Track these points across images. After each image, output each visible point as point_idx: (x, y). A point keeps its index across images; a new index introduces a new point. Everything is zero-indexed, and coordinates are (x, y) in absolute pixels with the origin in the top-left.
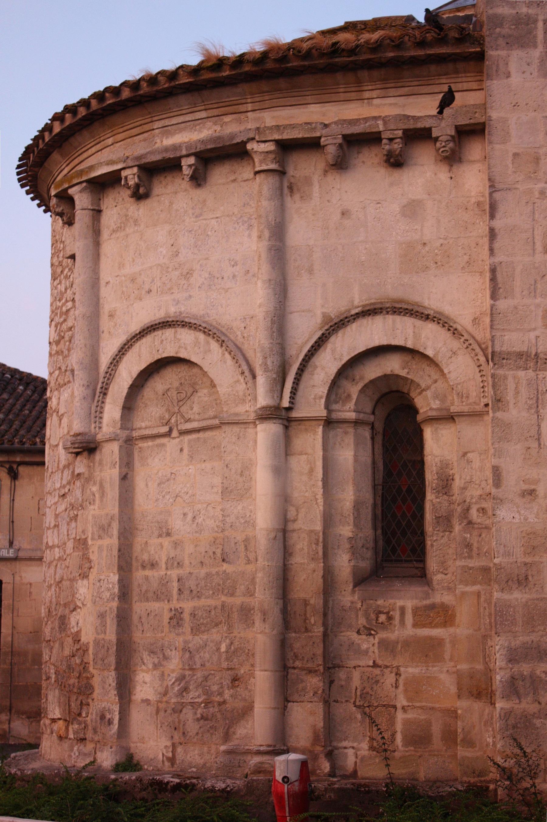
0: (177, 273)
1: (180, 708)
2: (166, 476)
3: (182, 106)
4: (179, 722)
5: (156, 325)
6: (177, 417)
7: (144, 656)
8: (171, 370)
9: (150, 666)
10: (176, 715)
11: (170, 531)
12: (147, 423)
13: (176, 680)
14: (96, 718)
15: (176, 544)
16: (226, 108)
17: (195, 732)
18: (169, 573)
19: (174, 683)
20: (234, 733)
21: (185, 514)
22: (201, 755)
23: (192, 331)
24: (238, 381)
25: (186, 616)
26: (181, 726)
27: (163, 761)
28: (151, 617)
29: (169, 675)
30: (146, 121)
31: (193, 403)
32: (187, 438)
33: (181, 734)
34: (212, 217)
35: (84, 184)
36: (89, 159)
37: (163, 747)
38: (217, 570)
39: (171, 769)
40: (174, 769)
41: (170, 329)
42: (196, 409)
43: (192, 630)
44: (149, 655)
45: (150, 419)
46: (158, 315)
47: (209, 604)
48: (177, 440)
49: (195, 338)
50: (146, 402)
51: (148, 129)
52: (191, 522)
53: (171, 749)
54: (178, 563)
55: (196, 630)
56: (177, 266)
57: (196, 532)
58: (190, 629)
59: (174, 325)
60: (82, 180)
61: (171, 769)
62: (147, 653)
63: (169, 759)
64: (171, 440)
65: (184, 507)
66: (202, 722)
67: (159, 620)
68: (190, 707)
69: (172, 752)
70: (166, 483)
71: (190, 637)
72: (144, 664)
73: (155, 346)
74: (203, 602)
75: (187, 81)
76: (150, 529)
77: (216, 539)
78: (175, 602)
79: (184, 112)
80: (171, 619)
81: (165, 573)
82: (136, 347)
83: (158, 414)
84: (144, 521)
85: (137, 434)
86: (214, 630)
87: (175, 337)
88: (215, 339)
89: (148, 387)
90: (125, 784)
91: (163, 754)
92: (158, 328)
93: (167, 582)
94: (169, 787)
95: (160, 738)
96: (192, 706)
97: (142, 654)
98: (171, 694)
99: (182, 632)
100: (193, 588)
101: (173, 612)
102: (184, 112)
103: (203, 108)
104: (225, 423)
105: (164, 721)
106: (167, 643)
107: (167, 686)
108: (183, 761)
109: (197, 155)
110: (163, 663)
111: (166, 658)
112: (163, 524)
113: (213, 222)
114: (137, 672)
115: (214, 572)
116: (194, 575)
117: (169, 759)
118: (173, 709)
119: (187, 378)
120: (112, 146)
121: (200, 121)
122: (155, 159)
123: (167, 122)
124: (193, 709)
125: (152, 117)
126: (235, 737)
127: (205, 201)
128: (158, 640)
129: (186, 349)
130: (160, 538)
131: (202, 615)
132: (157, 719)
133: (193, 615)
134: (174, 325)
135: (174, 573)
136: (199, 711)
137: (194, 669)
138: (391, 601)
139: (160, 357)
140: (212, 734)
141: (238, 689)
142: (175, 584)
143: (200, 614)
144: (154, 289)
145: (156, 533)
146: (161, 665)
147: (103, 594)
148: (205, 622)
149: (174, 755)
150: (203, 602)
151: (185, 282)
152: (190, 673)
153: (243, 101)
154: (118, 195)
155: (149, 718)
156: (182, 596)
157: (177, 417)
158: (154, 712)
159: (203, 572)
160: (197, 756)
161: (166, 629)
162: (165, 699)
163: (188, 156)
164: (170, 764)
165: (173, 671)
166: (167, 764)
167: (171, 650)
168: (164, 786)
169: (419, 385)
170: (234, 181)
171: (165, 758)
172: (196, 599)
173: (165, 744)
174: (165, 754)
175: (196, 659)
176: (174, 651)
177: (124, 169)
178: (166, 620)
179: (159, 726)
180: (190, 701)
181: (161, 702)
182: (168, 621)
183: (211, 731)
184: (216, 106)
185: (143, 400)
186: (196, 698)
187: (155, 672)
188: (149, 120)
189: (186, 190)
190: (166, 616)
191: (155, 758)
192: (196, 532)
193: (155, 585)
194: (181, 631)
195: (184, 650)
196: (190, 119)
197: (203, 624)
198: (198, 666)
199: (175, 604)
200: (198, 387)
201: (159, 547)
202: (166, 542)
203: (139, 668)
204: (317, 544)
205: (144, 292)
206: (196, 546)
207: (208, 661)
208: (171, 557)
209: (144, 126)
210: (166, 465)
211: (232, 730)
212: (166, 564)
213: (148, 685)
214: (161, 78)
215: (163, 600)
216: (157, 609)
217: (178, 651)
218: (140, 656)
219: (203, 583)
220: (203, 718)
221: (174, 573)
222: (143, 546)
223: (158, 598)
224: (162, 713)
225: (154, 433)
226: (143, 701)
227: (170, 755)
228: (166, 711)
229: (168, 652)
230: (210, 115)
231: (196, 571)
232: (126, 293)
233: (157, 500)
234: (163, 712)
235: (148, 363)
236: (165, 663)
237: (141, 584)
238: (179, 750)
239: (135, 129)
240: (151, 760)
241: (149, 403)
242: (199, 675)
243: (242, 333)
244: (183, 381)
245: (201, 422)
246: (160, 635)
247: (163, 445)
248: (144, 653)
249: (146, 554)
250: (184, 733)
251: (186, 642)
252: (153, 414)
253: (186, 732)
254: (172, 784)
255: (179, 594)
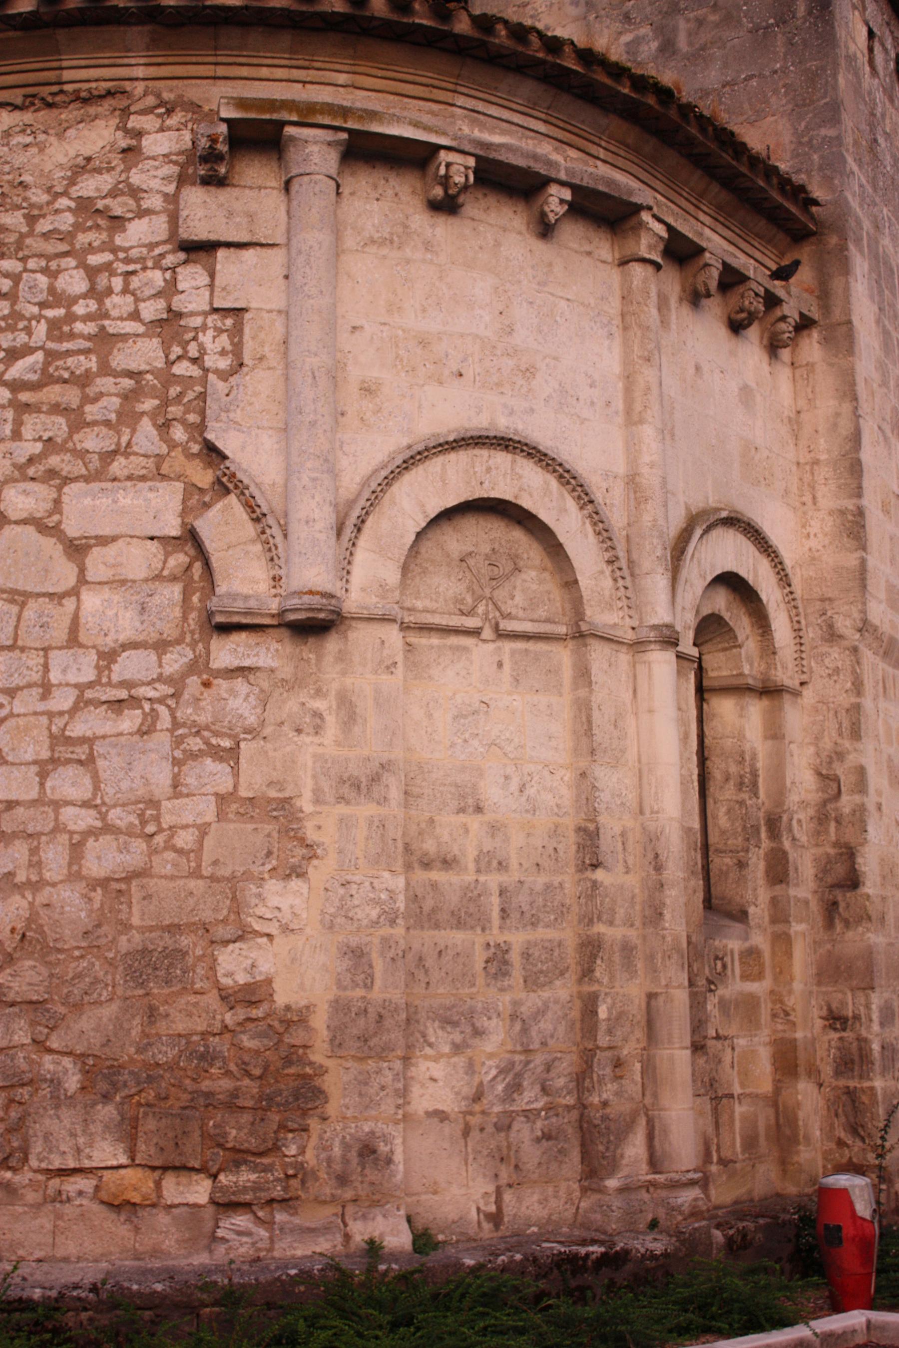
0: (511, 363)
1: (507, 1122)
2: (470, 705)
3: (515, 95)
4: (509, 1147)
5: (487, 437)
6: (487, 605)
7: (430, 1031)
8: (474, 522)
9: (446, 1049)
10: (503, 1134)
11: (481, 805)
12: (428, 604)
13: (500, 1072)
14: (344, 1157)
15: (494, 829)
16: (573, 137)
17: (536, 1161)
18: (482, 879)
19: (495, 1078)
20: (622, 1156)
21: (507, 778)
22: (543, 1202)
23: (539, 470)
24: (602, 572)
25: (515, 957)
26: (512, 1153)
27: (479, 1222)
28: (447, 958)
29: (484, 1063)
30: (444, 85)
31: (515, 588)
32: (508, 646)
33: (512, 1168)
34: (561, 294)
35: (345, 136)
36: (257, 83)
37: (479, 1196)
38: (559, 879)
39: (495, 1234)
40: (500, 1234)
41: (504, 454)
42: (519, 599)
43: (525, 981)
44: (443, 1028)
45: (434, 597)
46: (504, 424)
47: (549, 937)
48: (491, 646)
49: (545, 482)
50: (424, 565)
51: (441, 99)
52: (517, 793)
53: (493, 1199)
54: (500, 863)
55: (532, 982)
56: (510, 351)
57: (527, 811)
58: (521, 981)
59: (515, 448)
60: (345, 125)
61: (495, 1234)
62: (437, 1024)
63: (490, 1217)
64: (480, 643)
65: (505, 765)
66: (545, 1143)
67: (464, 964)
68: (523, 1119)
69: (496, 1203)
70: (470, 718)
71: (523, 995)
72: (430, 1045)
73: (475, 473)
74: (542, 933)
75: (574, 67)
76: (438, 795)
77: (557, 826)
78: (495, 931)
79: (514, 106)
80: (487, 962)
81: (475, 878)
82: (436, 464)
83: (451, 591)
84: (424, 780)
85: (412, 618)
86: (558, 983)
87: (512, 470)
88: (576, 494)
89: (429, 539)
90: (502, 1271)
91: (478, 1209)
92: (484, 444)
93: (479, 895)
94: (590, 1263)
95: (474, 1180)
96: (526, 1117)
97: (426, 1027)
98: (491, 1098)
99: (509, 986)
100: (525, 908)
101: (493, 950)
102: (514, 106)
103: (543, 116)
104: (596, 636)
105: (479, 1149)
106: (480, 1005)
107: (481, 1084)
108: (515, 1215)
109: (575, 188)
110: (470, 1042)
111: (478, 1033)
112: (467, 790)
113: (563, 304)
114: (413, 1061)
115: (556, 884)
116: (526, 886)
117: (490, 1217)
118: (495, 1124)
119: (503, 543)
120: (341, 89)
121: (532, 134)
122: (515, 162)
123: (480, 106)
124: (528, 1122)
125: (456, 84)
126: (624, 1162)
127: (550, 264)
128: (461, 999)
129: (531, 495)
130: (461, 815)
131: (540, 956)
132: (466, 1146)
133: (526, 955)
134: (515, 448)
135: (493, 880)
136: (539, 1124)
137: (530, 1051)
138: (724, 941)
139: (486, 496)
140: (561, 1162)
141: (623, 1082)
142: (495, 900)
143: (537, 954)
144: (469, 374)
145: (454, 804)
146: (468, 1046)
147: (357, 910)
148: (544, 968)
149: (499, 1208)
150: (542, 933)
151: (523, 382)
152: (523, 1058)
153: (596, 140)
154: (383, 182)
155: (446, 1145)
156: (508, 921)
157: (487, 605)
158: (459, 1133)
159: (540, 881)
160: (536, 1205)
161: (480, 980)
162: (477, 1108)
163: (563, 184)
164: (491, 1225)
165: (491, 1056)
166: (487, 1226)
167: (490, 1018)
168: (581, 1262)
169: (736, 637)
170: (589, 254)
171: (482, 1216)
172: (529, 928)
173: (484, 1190)
174: (483, 1208)
175: (534, 1034)
176: (495, 1021)
177: (449, 149)
178: (479, 965)
179: (471, 1157)
180: (524, 1107)
181: (471, 1113)
182: (483, 965)
183: (560, 1159)
184: (561, 124)
185: (418, 561)
186: (533, 1102)
187: (455, 1059)
188: (451, 86)
189: (520, 233)
190: (479, 957)
191: (461, 1218)
192: (527, 811)
193: (453, 899)
194: (506, 983)
195: (514, 1017)
196: (521, 123)
197: (541, 972)
198: (535, 1045)
199: (496, 936)
200: (521, 564)
201: (461, 831)
202: (475, 823)
203: (418, 1054)
204: (695, 850)
205: (446, 372)
206: (528, 835)
207: (552, 1036)
208: (485, 851)
209: (435, 91)
210: (471, 684)
211: (619, 1151)
212: (477, 861)
213: (441, 1083)
214: (534, 38)
215: (472, 928)
216: (459, 943)
217: (503, 1020)
218: (419, 1031)
219: (540, 901)
220: (547, 1136)
221: (493, 880)
222: (423, 825)
223: (460, 924)
224: (475, 1134)
225: (451, 624)
226: (430, 1114)
227: (493, 1208)
228: (482, 1130)
229: (482, 1022)
230: (551, 134)
231: (531, 879)
232: (405, 361)
233: (453, 745)
234: (478, 1132)
235: (462, 499)
236: (476, 1042)
237: (420, 896)
238: (508, 1197)
239: (412, 86)
240: (453, 1222)
241: (431, 569)
242: (539, 1060)
243: (604, 498)
244: (497, 546)
245: (536, 624)
246: (467, 991)
247: (466, 649)
248: (428, 1025)
249: (430, 842)
250: (516, 1166)
251: (516, 1003)
252: (441, 589)
253: (520, 1164)
254: (594, 1256)
255: (503, 918)
